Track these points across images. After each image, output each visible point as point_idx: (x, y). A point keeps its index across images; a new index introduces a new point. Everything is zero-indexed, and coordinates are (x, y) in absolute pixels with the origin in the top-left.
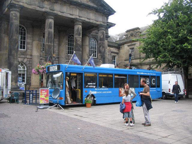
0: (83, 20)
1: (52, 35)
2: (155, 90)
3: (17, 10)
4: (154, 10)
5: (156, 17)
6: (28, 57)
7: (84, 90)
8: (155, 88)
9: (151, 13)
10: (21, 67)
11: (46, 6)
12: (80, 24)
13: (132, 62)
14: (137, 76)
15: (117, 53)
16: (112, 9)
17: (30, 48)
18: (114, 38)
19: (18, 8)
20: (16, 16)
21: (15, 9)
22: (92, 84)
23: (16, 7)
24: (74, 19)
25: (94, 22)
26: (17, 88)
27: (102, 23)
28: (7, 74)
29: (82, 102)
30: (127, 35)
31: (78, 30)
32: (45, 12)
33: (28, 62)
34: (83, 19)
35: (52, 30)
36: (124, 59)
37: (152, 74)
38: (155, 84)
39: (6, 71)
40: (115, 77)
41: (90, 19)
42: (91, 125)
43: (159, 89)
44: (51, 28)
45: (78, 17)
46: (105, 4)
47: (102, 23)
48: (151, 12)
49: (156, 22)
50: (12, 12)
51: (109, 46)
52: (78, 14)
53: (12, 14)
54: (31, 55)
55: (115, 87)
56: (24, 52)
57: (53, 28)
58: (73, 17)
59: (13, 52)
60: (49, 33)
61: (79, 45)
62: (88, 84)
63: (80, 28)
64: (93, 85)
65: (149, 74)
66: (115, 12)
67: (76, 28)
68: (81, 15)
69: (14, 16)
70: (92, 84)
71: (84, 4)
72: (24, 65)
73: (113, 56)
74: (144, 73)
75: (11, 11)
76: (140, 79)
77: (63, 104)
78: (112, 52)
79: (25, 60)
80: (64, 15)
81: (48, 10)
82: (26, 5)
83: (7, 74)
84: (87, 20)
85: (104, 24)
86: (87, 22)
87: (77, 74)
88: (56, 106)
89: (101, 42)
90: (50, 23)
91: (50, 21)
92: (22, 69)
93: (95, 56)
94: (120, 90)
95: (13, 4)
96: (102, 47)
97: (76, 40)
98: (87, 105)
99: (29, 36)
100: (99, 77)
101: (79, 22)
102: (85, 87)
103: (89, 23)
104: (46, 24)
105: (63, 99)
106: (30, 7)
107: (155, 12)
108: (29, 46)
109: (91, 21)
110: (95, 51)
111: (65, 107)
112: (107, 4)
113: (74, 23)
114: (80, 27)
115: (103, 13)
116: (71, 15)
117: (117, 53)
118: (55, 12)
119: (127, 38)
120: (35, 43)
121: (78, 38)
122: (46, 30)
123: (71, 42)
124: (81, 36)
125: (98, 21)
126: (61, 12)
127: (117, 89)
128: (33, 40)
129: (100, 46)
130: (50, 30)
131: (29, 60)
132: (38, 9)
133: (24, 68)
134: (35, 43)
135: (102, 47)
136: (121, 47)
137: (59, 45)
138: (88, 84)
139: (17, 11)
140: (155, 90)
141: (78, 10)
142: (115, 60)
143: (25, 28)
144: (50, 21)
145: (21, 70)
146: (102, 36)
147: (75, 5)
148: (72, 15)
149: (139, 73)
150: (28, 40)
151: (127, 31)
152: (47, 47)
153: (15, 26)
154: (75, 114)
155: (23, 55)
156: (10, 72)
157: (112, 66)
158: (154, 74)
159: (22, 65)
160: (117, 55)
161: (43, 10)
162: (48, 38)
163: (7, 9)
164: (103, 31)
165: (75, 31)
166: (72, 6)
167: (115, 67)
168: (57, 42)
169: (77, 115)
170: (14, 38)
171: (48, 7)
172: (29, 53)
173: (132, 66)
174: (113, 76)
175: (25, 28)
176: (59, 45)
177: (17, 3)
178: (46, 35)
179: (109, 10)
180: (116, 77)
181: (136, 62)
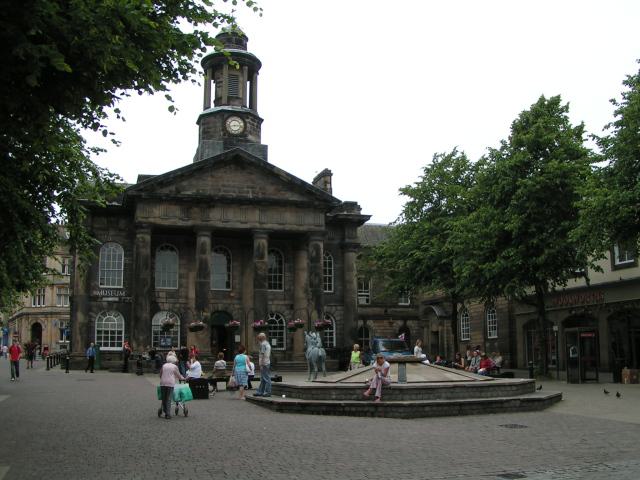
3: (146, 230)
6: (181, 300)
20: (144, 241)
31: (259, 247)
41: (283, 224)
45: (258, 225)
50: (138, 236)
68: (264, 220)
80: (228, 225)
85: (317, 228)
91: (262, 242)
93: (330, 289)
109: (288, 227)
110: (330, 279)
116: (242, 223)
123: (114, 259)
139: (147, 233)
141: (257, 212)
144: (262, 242)
154: (518, 430)
164: (315, 242)
166: (244, 207)
169: (515, 426)
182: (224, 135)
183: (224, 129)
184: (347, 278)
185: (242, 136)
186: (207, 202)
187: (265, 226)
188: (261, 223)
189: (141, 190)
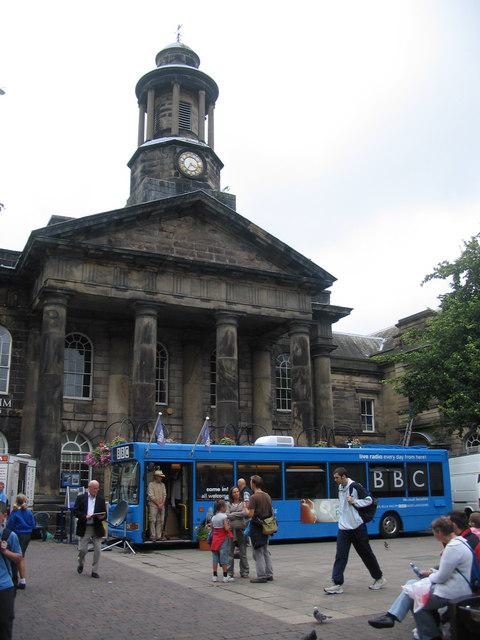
0: (240, 312)
1: (151, 360)
2: (426, 502)
3: (61, 301)
4: (439, 267)
5: (445, 286)
6: (96, 417)
7: (196, 504)
8: (426, 499)
9: (432, 276)
10: (74, 442)
11: (134, 284)
12: (232, 324)
13: (419, 418)
14: (362, 464)
15: (377, 393)
16: (324, 272)
17: (102, 394)
18: (366, 346)
19: (62, 297)
20: (56, 317)
21: (55, 301)
22: (219, 490)
23: (57, 296)
24: (214, 310)
25: (274, 313)
26: (53, 503)
27: (297, 314)
28: (23, 467)
29: (190, 537)
30: (400, 335)
31: (226, 338)
32: (132, 300)
33: (97, 432)
34: (239, 308)
35: (153, 347)
36: (396, 408)
37: (411, 457)
38: (426, 484)
39: (20, 459)
40: (288, 470)
42: (274, 619)
43: (439, 501)
44: (147, 340)
45: (224, 305)
46: (301, 262)
47: (297, 314)
48: (433, 272)
49: (447, 301)
50: (47, 308)
51: (335, 370)
52: (224, 297)
53: (48, 313)
54: (105, 413)
55: (290, 497)
56: (85, 405)
57: (154, 339)
58: (210, 305)
59: (49, 409)
60: (145, 355)
61: (229, 381)
62: (208, 490)
63: (232, 333)
64: (221, 493)
65: (401, 458)
66: (335, 279)
67: (221, 334)
68: (232, 298)
69: (54, 318)
70: (219, 490)
71: (238, 269)
72: (87, 441)
73: (363, 403)
74: (383, 455)
75: (46, 305)
76: (371, 474)
77: (139, 540)
78: (358, 391)
79: (90, 427)
80: (184, 302)
81: (141, 295)
82: (81, 288)
83: (23, 467)
84: (250, 310)
85: (302, 316)
86: (252, 317)
87: (182, 464)
88: (121, 545)
89: (297, 367)
90: (147, 328)
91: (147, 322)
92: (80, 452)
94: (304, 504)
95: (51, 287)
96: (299, 383)
97: (222, 367)
98: (202, 544)
99: (100, 360)
100: (286, 473)
101: (228, 318)
102: (199, 499)
103: (259, 317)
104: (136, 331)
105: (140, 529)
106: (92, 291)
107: (444, 271)
108: (100, 388)
109: (265, 312)
111: (141, 548)
112: (308, 261)
113: (215, 320)
114: (233, 330)
115: (300, 286)
116: (203, 300)
117: (377, 393)
118: (159, 297)
119: (400, 345)
120: (115, 379)
121: (229, 363)
122: (136, 347)
124: (236, 357)
125: (284, 311)
126: (175, 296)
127: (295, 503)
128: (110, 372)
129: (296, 380)
130: (146, 346)
131: (98, 425)
132: (113, 293)
133: (86, 447)
134: (115, 379)
135: (299, 383)
136: (387, 371)
137: (184, 381)
138: (208, 490)
140: (426, 502)
141: (223, 286)
142: (370, 412)
143: (90, 341)
144: (147, 322)
145: (78, 455)
146: (300, 350)
147: (213, 273)
148: (208, 300)
149: (367, 457)
150: (97, 373)
151: (402, 323)
152: (138, 392)
153: (54, 342)
155: (85, 413)
156: (32, 463)
157: (288, 441)
158: (419, 457)
159: (81, 440)
160: (375, 398)
161: (128, 295)
162: (142, 367)
163: (38, 301)
165: (218, 343)
166: (205, 278)
167: (297, 444)
168: (178, 374)
170: (52, 372)
171: (140, 285)
172: (99, 408)
173: (420, 430)
174: (281, 467)
175: (90, 341)
176: (184, 381)
177: (60, 285)
178: (137, 361)
179: (315, 276)
180: (200, 465)
181: (430, 416)
182: (177, 174)
183: (177, 167)
184: (322, 392)
185: (200, 179)
186: (154, 264)
187: (235, 307)
188: (229, 303)
189: (58, 236)
